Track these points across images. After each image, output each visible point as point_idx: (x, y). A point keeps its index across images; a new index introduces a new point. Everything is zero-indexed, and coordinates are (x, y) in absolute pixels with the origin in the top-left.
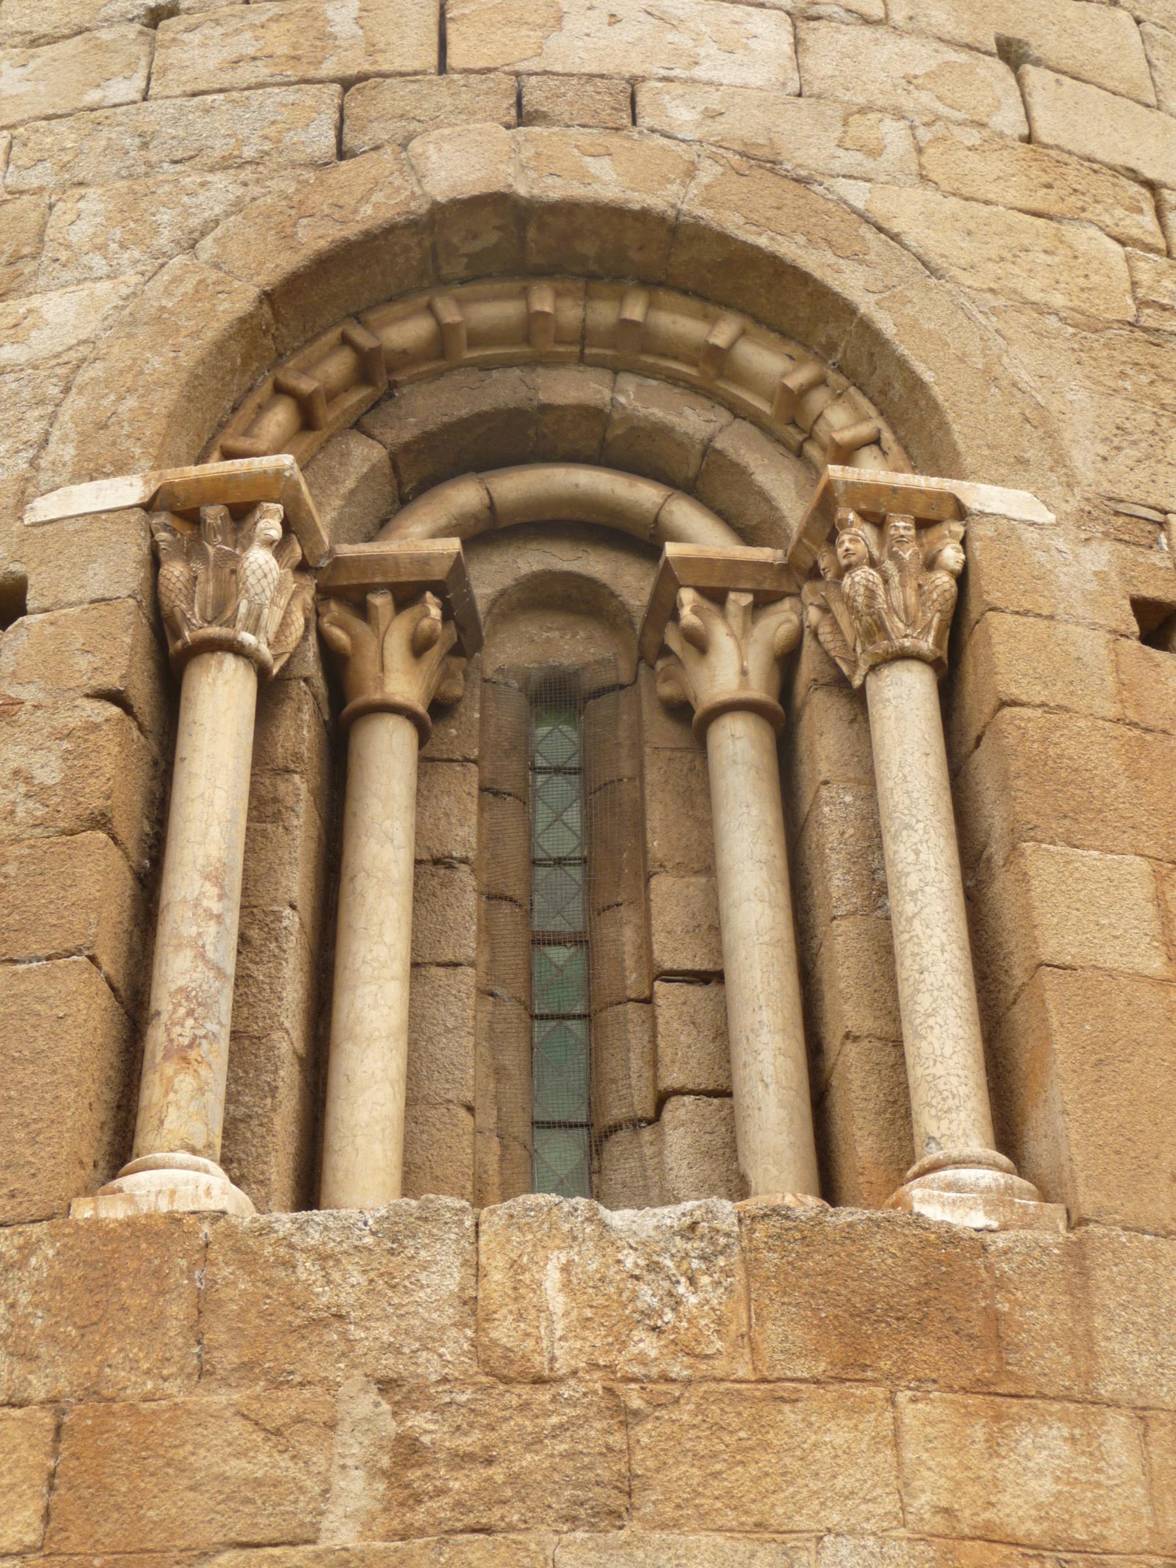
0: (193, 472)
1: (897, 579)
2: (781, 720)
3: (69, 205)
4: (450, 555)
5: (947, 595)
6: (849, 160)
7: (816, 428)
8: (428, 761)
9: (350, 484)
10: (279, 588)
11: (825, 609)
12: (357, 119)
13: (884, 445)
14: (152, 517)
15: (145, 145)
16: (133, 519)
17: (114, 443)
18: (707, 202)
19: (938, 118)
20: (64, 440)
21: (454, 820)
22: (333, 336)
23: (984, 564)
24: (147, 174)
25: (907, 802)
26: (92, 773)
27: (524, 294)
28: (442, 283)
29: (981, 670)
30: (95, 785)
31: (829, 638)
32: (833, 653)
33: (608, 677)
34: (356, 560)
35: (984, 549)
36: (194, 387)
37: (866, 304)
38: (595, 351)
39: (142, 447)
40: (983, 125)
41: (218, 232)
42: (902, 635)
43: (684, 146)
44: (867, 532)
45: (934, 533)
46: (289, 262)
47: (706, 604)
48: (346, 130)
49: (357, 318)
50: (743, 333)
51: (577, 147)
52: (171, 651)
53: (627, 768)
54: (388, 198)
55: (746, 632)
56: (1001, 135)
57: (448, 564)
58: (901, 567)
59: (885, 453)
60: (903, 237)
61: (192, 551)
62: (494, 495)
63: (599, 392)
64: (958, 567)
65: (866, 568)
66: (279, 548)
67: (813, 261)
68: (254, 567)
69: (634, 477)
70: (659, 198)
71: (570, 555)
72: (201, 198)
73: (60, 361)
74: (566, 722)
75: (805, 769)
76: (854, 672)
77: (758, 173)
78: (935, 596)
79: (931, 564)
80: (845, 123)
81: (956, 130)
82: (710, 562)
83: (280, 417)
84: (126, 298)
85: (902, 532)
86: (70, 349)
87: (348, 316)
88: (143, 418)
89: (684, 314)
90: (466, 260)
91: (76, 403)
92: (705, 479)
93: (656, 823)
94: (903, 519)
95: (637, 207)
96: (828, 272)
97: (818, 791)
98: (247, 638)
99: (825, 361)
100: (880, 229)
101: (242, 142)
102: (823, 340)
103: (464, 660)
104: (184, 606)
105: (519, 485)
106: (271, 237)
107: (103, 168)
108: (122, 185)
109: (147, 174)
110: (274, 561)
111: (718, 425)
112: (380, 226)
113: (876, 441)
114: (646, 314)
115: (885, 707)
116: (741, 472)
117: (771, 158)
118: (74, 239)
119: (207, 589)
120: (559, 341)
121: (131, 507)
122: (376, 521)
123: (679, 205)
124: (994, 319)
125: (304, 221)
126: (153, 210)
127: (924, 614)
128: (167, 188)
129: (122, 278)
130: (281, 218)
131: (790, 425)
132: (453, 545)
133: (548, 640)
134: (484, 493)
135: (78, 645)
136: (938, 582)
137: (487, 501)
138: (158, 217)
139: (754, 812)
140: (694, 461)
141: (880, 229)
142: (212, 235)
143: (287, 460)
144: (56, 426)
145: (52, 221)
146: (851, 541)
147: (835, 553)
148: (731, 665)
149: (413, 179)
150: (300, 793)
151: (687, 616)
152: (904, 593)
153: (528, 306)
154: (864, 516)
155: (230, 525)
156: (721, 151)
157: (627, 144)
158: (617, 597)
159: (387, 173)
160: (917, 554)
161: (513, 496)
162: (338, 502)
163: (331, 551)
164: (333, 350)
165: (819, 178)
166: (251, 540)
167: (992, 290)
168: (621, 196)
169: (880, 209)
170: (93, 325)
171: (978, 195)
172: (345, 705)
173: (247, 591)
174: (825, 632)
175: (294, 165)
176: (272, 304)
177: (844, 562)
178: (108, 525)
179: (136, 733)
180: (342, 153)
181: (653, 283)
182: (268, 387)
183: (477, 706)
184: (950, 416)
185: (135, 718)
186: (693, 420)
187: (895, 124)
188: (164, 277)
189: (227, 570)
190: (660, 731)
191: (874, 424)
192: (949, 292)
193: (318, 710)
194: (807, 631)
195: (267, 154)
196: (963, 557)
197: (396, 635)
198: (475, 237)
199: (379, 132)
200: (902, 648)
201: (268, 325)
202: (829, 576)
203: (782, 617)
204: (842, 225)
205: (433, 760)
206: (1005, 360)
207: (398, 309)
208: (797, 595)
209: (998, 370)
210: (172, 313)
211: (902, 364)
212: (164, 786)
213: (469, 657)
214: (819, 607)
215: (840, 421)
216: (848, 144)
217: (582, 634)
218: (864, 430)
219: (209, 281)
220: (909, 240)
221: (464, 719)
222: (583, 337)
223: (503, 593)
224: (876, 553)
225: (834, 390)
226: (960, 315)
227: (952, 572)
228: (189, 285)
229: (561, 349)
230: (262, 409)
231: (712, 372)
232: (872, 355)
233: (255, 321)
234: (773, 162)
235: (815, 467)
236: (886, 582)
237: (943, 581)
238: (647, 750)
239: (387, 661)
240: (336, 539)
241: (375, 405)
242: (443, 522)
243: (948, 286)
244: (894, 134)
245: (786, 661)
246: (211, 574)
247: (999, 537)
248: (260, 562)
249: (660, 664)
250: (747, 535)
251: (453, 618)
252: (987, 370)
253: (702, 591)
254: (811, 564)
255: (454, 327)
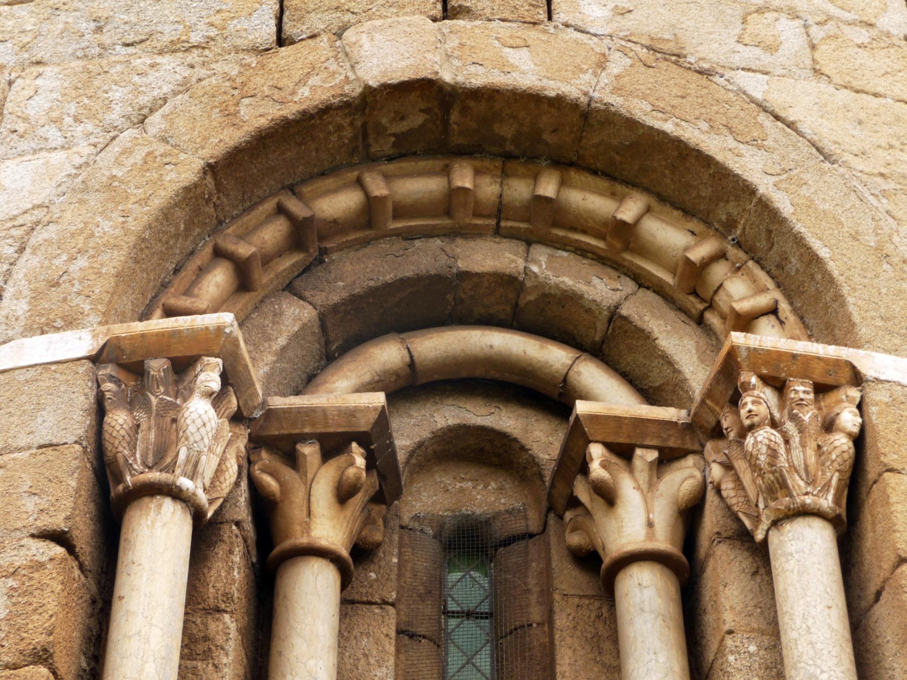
0: (139, 327)
1: (797, 440)
2: (686, 571)
3: (28, 82)
4: (375, 409)
5: (846, 456)
6: (748, 55)
7: (717, 298)
8: (349, 603)
9: (282, 341)
10: (216, 438)
11: (728, 467)
12: (296, 9)
13: (781, 315)
14: (98, 369)
15: (99, 29)
16: (81, 370)
17: (65, 300)
18: (617, 90)
19: (830, 18)
20: (17, 296)
21: (372, 661)
22: (269, 206)
23: (880, 427)
24: (100, 55)
25: (812, 653)
26: (35, 610)
27: (446, 171)
28: (372, 160)
29: (879, 528)
30: (39, 621)
31: (732, 493)
32: (736, 508)
33: (517, 526)
34: (287, 411)
35: (880, 413)
36: (141, 250)
37: (765, 186)
38: (510, 224)
39: (91, 303)
40: (871, 25)
41: (166, 109)
42: (802, 492)
43: (595, 39)
44: (769, 394)
45: (832, 398)
46: (232, 137)
47: (614, 459)
48: (285, 19)
49: (292, 189)
50: (648, 210)
51: (497, 38)
52: (112, 494)
53: (536, 614)
54: (324, 82)
55: (651, 486)
56: (888, 35)
57: (373, 417)
58: (801, 430)
59: (782, 323)
60: (798, 125)
61: (136, 400)
62: (415, 354)
63: (513, 261)
64: (856, 430)
65: (768, 429)
66: (217, 399)
67: (715, 145)
68: (194, 416)
69: (543, 339)
70: (572, 87)
71: (483, 410)
72: (151, 78)
73: (16, 223)
74: (477, 569)
75: (709, 618)
76: (757, 527)
77: (664, 65)
78: (834, 456)
79: (829, 426)
80: (744, 22)
81: (847, 29)
82: (618, 420)
83: (218, 279)
84: (80, 167)
85: (802, 396)
86: (25, 212)
87: (283, 188)
88: (93, 277)
89: (593, 192)
90: (393, 139)
91: (29, 262)
92: (613, 343)
93: (566, 668)
94: (802, 384)
95: (552, 94)
96: (730, 155)
97: (723, 640)
98: (185, 483)
99: (725, 237)
100: (777, 118)
101: (190, 28)
102: (724, 217)
103: (384, 507)
104: (126, 452)
105: (438, 345)
106: (216, 114)
107: (60, 48)
108: (77, 65)
109: (100, 55)
110: (213, 411)
111: (624, 294)
112: (316, 107)
113: (774, 311)
114: (558, 192)
115: (787, 561)
116: (645, 337)
117: (676, 51)
118: (31, 112)
119: (149, 436)
120: (477, 215)
121: (79, 359)
122: (304, 376)
123: (591, 93)
124: (885, 201)
125: (246, 101)
126: (106, 88)
127: (824, 473)
128: (119, 68)
129: (75, 149)
130: (225, 97)
131: (691, 292)
132: (379, 399)
133: (462, 490)
134: (405, 352)
135: (26, 488)
136: (836, 443)
137: (408, 359)
138: (110, 94)
139: (662, 659)
140: (601, 326)
141: (777, 118)
142: (160, 112)
143: (227, 318)
144: (10, 283)
145: (11, 96)
146: (753, 402)
147: (738, 414)
148: (638, 517)
149: (348, 65)
150: (229, 630)
151: (597, 470)
152: (804, 453)
153: (449, 182)
154: (766, 380)
155: (172, 377)
156: (630, 45)
157: (544, 37)
158: (527, 450)
159: (323, 59)
160: (816, 416)
161: (432, 355)
162: (270, 358)
163: (264, 403)
164: (269, 218)
165: (720, 71)
166: (191, 391)
167: (882, 175)
168: (538, 84)
169: (777, 99)
170: (48, 191)
171: (867, 88)
172: (272, 548)
173: (187, 439)
174: (728, 488)
175: (237, 50)
176: (215, 176)
177: (747, 422)
178: (58, 376)
179: (77, 572)
180: (281, 40)
181: (566, 163)
182: (209, 250)
183: (396, 551)
184: (845, 290)
185: (77, 558)
186: (600, 289)
187: (790, 23)
188: (115, 148)
189: (169, 419)
190: (568, 578)
191: (773, 295)
192: (842, 176)
193: (247, 554)
194: (710, 487)
195: (213, 39)
196: (860, 420)
197: (323, 482)
198: (403, 119)
199: (316, 22)
200: (804, 505)
201: (210, 194)
202: (732, 435)
203: (686, 473)
204: (742, 114)
205: (353, 602)
206: (896, 239)
207: (330, 182)
208: (700, 452)
209: (889, 249)
210: (121, 182)
211: (799, 241)
212: (100, 623)
213: (389, 505)
214: (721, 464)
215: (739, 291)
216: (747, 40)
217: (493, 485)
218: (763, 301)
219: (157, 153)
220: (804, 127)
221: (383, 563)
222: (500, 211)
223: (420, 445)
224: (777, 415)
225: (733, 264)
226: (853, 196)
227: (850, 435)
228: (138, 157)
229: (479, 222)
230: (202, 271)
231: (618, 245)
232: (771, 232)
233: (199, 191)
234: (678, 56)
235: (715, 334)
236: (787, 442)
237: (842, 443)
238: (557, 597)
239: (314, 506)
240: (267, 393)
241: (307, 269)
242: (367, 378)
243: (841, 170)
244: (789, 33)
245: (690, 515)
246: (153, 422)
247: (894, 402)
248: (200, 414)
249: (568, 515)
250: (650, 396)
251: (375, 467)
252: (879, 248)
253: (609, 446)
254: (714, 423)
255: (382, 200)
